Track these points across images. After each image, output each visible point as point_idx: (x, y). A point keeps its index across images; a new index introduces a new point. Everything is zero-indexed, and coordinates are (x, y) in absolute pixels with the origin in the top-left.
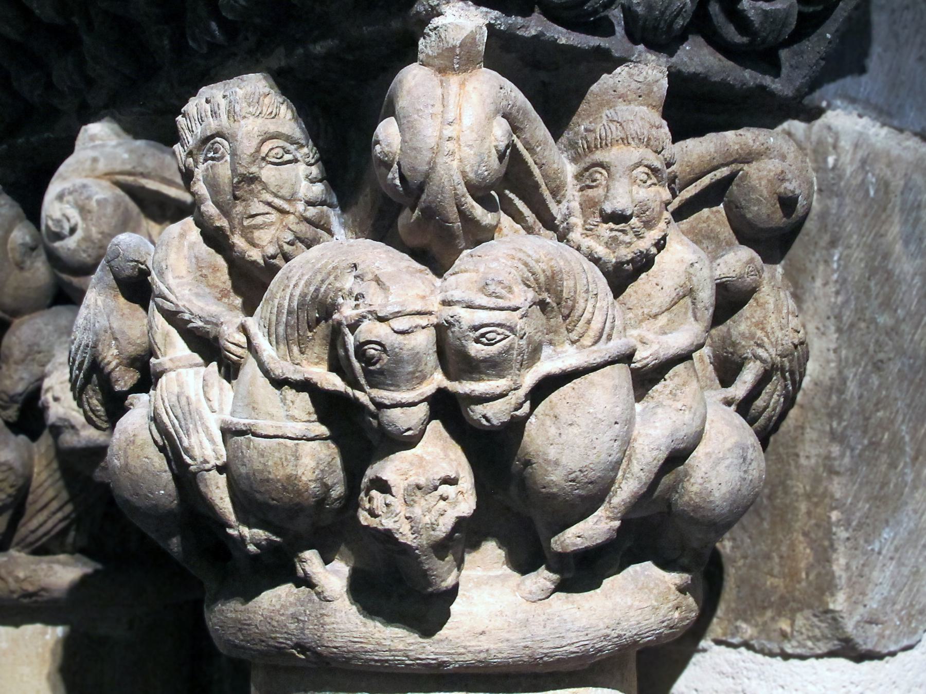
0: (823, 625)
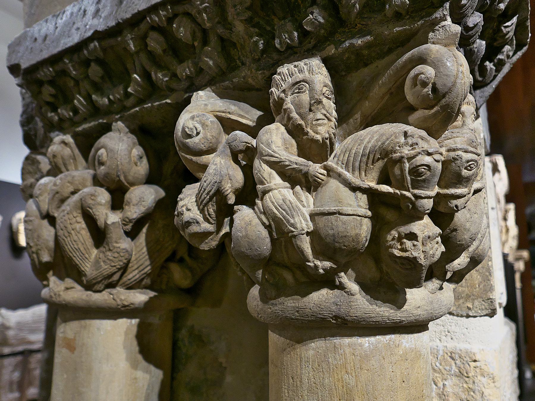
0: (486, 304)
